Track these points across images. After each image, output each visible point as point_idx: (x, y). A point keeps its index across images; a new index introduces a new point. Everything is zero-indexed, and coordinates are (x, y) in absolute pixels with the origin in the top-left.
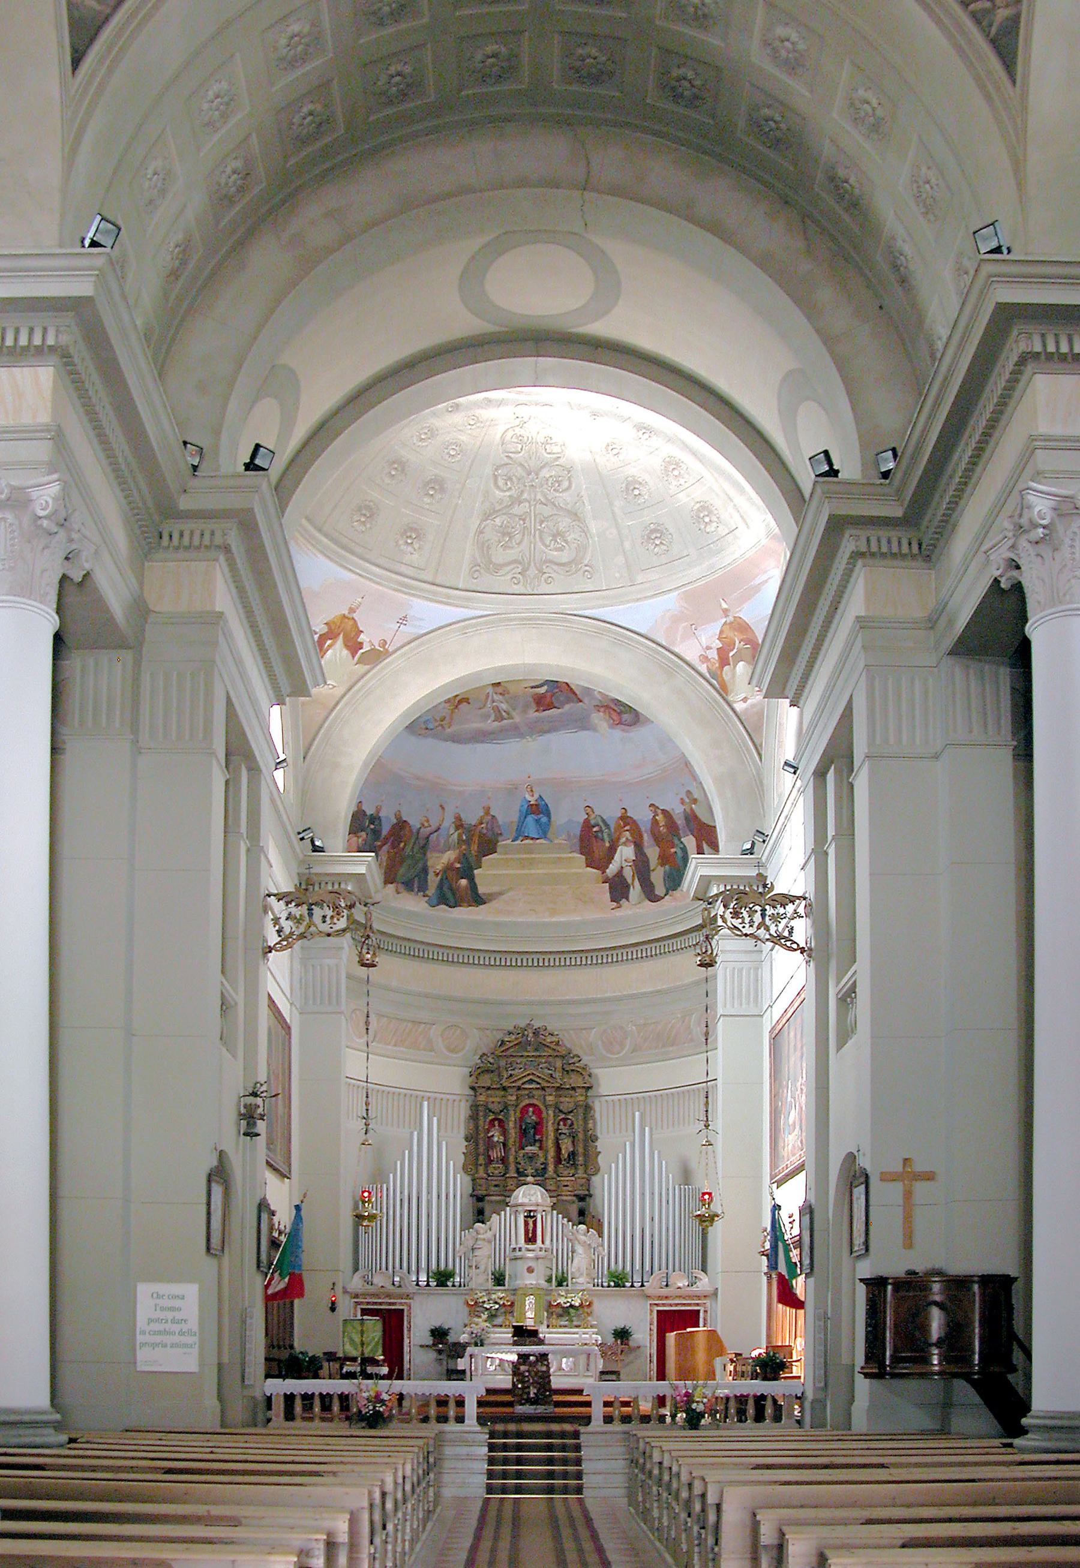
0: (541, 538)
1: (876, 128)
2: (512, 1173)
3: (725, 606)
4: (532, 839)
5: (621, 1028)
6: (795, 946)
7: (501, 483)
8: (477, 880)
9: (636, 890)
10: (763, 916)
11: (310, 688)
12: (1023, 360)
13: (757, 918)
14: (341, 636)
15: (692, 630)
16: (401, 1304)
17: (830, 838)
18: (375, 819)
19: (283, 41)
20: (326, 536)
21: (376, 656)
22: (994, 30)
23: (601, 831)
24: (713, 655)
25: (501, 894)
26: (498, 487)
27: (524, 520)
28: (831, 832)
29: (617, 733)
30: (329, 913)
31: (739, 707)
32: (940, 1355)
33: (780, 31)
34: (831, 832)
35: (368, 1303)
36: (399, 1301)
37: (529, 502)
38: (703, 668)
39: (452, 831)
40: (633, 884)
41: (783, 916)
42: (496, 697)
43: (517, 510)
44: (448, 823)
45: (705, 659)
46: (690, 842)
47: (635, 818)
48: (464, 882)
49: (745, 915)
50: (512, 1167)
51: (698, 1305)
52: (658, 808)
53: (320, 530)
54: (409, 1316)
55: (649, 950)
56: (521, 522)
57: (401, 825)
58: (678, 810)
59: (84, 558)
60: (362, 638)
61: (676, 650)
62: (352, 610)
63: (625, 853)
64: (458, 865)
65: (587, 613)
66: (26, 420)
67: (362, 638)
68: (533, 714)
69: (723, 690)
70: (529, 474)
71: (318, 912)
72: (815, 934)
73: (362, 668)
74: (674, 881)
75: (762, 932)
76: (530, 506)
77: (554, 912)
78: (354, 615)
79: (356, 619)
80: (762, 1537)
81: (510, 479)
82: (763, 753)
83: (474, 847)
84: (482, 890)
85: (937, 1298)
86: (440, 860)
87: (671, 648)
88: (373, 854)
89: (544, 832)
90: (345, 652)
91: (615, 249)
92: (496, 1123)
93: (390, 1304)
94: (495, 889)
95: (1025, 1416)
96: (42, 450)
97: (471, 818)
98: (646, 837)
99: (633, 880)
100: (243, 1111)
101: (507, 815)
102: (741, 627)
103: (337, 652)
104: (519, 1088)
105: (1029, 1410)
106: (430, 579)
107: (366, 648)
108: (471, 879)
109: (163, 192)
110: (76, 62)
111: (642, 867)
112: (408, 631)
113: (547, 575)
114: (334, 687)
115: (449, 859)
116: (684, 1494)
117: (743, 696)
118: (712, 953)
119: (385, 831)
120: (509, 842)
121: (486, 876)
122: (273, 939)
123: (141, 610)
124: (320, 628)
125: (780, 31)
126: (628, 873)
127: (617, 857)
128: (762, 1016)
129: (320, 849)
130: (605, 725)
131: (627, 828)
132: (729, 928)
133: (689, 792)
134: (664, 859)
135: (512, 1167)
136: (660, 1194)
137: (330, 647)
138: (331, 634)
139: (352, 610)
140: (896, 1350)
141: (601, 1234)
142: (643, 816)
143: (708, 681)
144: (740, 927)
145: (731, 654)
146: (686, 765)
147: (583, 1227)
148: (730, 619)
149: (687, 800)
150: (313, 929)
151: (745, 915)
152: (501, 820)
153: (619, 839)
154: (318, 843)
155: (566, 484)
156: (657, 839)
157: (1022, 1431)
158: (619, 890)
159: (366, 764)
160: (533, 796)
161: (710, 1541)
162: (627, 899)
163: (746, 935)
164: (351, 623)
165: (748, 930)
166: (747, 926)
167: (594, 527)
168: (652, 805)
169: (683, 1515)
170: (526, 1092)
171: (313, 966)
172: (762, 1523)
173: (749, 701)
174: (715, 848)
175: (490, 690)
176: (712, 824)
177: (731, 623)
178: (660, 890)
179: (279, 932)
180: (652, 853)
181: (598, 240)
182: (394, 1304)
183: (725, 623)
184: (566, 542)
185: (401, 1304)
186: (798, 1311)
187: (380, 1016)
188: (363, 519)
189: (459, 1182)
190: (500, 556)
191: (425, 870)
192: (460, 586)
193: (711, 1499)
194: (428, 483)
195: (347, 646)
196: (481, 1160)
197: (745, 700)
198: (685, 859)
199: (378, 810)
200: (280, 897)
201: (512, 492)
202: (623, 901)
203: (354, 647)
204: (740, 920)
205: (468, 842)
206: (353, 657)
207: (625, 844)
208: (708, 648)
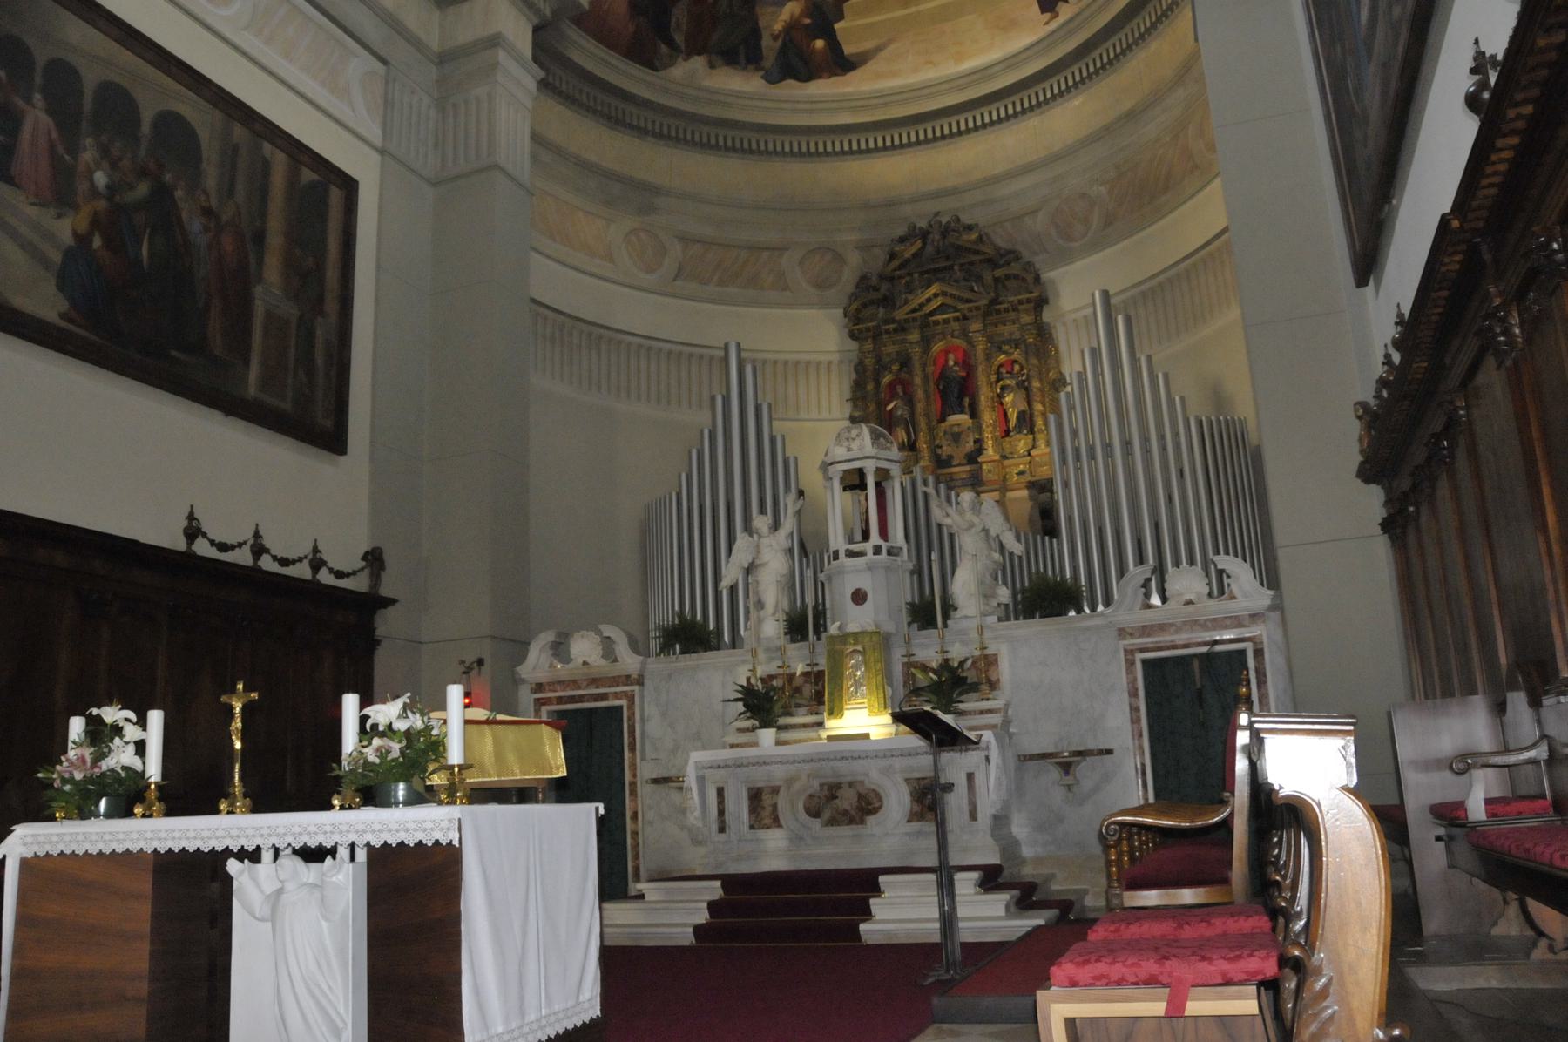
5: (1083, 195)
16: (617, 696)
25: (878, 49)
48: (820, 44)
54: (631, 717)
64: (807, 21)
77: (959, 57)
84: (849, 49)
92: (899, 390)
94: (868, 45)
136: (1162, 437)
171: (454, 105)
182: (603, 697)
185: (617, 696)
189: (1347, 720)
191: (756, 33)
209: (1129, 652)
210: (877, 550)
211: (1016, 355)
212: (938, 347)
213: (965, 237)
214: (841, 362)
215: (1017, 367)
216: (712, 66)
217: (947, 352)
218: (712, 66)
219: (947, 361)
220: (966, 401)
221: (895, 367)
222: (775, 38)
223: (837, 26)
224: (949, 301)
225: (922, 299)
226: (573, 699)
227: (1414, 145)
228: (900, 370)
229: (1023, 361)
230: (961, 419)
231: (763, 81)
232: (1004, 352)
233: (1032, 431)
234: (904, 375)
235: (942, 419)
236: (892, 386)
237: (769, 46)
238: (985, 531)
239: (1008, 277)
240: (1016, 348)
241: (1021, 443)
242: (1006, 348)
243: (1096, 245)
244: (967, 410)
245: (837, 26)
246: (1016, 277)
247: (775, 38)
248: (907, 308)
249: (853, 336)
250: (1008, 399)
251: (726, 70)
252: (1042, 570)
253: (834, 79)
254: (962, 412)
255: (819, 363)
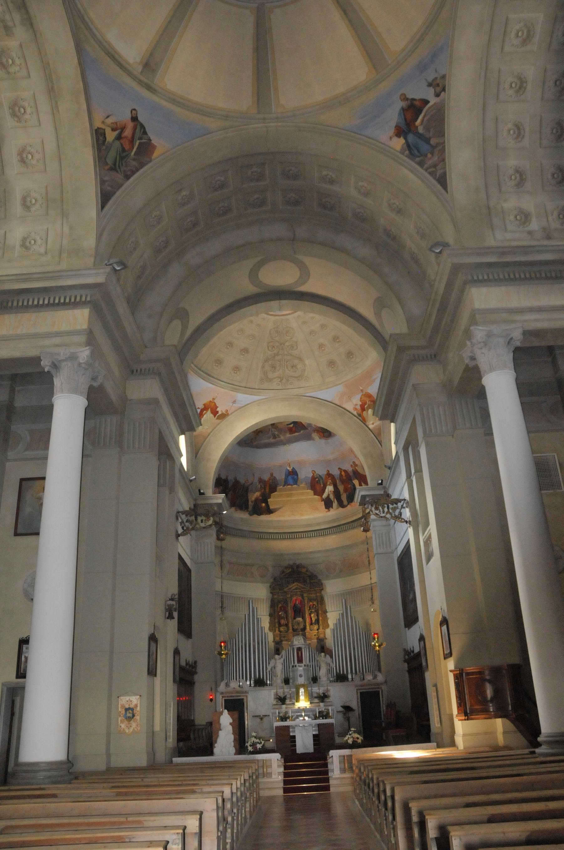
0: (287, 368)
1: (399, 211)
2: (291, 630)
3: (361, 388)
4: (291, 485)
6: (403, 520)
7: (270, 348)
8: (269, 503)
9: (335, 504)
10: (388, 508)
11: (195, 427)
12: (465, 283)
13: (386, 510)
14: (210, 410)
15: (350, 399)
17: (413, 474)
18: (226, 481)
19: (180, 198)
20: (203, 371)
21: (223, 416)
22: (438, 176)
23: (319, 480)
24: (358, 407)
25: (280, 508)
26: (269, 350)
27: (280, 362)
28: (413, 471)
29: (323, 441)
30: (204, 518)
31: (371, 427)
32: (492, 706)
33: (361, 184)
34: (413, 471)
35: (228, 697)
36: (242, 694)
37: (282, 355)
38: (355, 413)
39: (258, 484)
40: (334, 501)
41: (397, 508)
42: (273, 429)
43: (277, 358)
44: (256, 480)
45: (355, 409)
46: (356, 482)
47: (333, 474)
48: (264, 505)
49: (380, 508)
50: (291, 628)
51: (378, 688)
52: (342, 469)
53: (200, 370)
55: (343, 528)
56: (279, 362)
57: (236, 482)
58: (350, 469)
59: (99, 378)
60: (218, 409)
61: (344, 406)
62: (214, 399)
63: (330, 489)
64: (261, 498)
65: (307, 395)
66: (78, 327)
67: (218, 409)
68: (288, 435)
69: (364, 421)
70: (281, 345)
71: (199, 519)
72: (411, 515)
73: (219, 421)
74: (351, 499)
75: (388, 516)
76: (282, 357)
78: (215, 401)
79: (216, 403)
80: (413, 817)
81: (274, 347)
82: (382, 444)
83: (267, 490)
84: (271, 507)
85: (488, 677)
86: (254, 496)
87: (342, 406)
88: (224, 495)
89: (296, 482)
90: (212, 415)
91: (307, 260)
93: (238, 696)
94: (277, 507)
95: (539, 736)
96: (83, 338)
97: (266, 477)
98: (338, 481)
99: (334, 500)
100: (167, 607)
101: (280, 476)
102: (369, 396)
103: (208, 415)
104: (291, 592)
105: (540, 733)
106: (245, 386)
107: (220, 413)
108: (267, 503)
109: (135, 249)
110: (103, 207)
111: (337, 493)
112: (236, 405)
113: (290, 381)
114: (207, 429)
115: (257, 496)
116: (376, 790)
117: (371, 422)
118: (368, 526)
119: (230, 485)
120: (281, 487)
121: (273, 502)
122: (180, 531)
123: (124, 400)
124: (202, 406)
125: (361, 184)
126: (332, 497)
127: (327, 490)
128: (393, 553)
129: (203, 494)
130: (318, 438)
131: (330, 478)
132: (374, 515)
133: (354, 462)
134: (346, 490)
135: (291, 628)
137: (205, 413)
138: (206, 408)
139: (214, 399)
140: (471, 705)
141: (331, 657)
142: (335, 472)
143: (357, 417)
144: (379, 513)
145: (366, 406)
146: (352, 451)
147: (323, 654)
148: (364, 393)
149: (353, 465)
150: (197, 526)
151: (380, 508)
152: (277, 478)
153: (327, 482)
154: (202, 491)
155: (295, 347)
156: (342, 481)
157: (538, 745)
158: (328, 504)
159: (221, 459)
160: (290, 468)
161: (390, 817)
162: (332, 508)
163: (382, 517)
164: (213, 404)
165: (382, 515)
166: (382, 513)
167: (307, 362)
168: (339, 468)
169: (377, 802)
170: (294, 593)
172: (412, 808)
173: (375, 424)
174: (367, 484)
175: (270, 427)
176: (365, 474)
177: (364, 395)
178: (345, 502)
179: (183, 528)
180: (341, 488)
181: (300, 257)
182: (240, 696)
183: (362, 395)
184: (297, 369)
185: (243, 696)
186: (220, 590)
187: (230, 563)
188: (217, 365)
190: (271, 375)
192: (257, 388)
193: (389, 793)
194: (243, 350)
195: (212, 413)
196: (277, 625)
197: (373, 424)
198: (355, 489)
199: (227, 477)
200: (183, 513)
201: (275, 352)
202: (331, 509)
203: (215, 413)
204: (378, 511)
205: (265, 488)
206: (215, 417)
207: (329, 485)
208: (356, 405)
209: (357, 690)
210: (305, 666)
211: (315, 603)
212: (294, 598)
213: (303, 570)
214: (266, 599)
215: (315, 606)
216: (236, 510)
217: (296, 600)
218: (236, 510)
219: (296, 602)
220: (301, 614)
221: (282, 603)
222: (252, 502)
223: (269, 500)
224: (298, 587)
225: (292, 586)
226: (231, 696)
227: (402, 750)
228: (284, 604)
229: (316, 605)
230: (300, 619)
231: (248, 515)
232: (311, 602)
233: (318, 624)
234: (284, 605)
235: (295, 618)
236: (281, 608)
237: (251, 504)
238: (327, 662)
239: (314, 582)
240: (315, 601)
241: (316, 627)
242: (312, 601)
243: (337, 577)
244: (301, 616)
245: (269, 500)
246: (316, 583)
247: (252, 502)
248: (288, 588)
249: (271, 593)
250: (312, 615)
251: (239, 511)
252: (338, 672)
253: (267, 515)
254: (300, 617)
255: (261, 599)
